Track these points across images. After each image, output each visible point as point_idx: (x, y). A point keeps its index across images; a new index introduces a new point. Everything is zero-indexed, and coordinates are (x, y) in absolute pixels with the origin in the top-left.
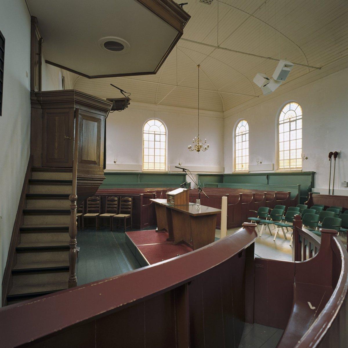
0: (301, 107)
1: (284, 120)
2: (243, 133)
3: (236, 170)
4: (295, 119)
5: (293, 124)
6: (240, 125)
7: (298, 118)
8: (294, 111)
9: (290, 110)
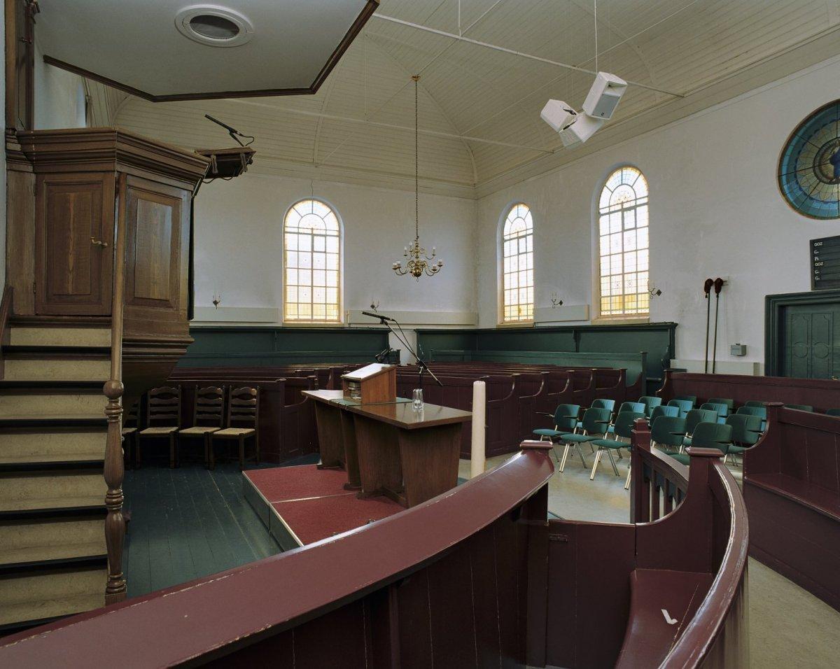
0: (646, 178)
1: (609, 207)
2: (520, 234)
3: (603, 313)
4: (633, 204)
5: (629, 215)
6: (512, 214)
7: (639, 202)
8: (632, 187)
9: (622, 184)
